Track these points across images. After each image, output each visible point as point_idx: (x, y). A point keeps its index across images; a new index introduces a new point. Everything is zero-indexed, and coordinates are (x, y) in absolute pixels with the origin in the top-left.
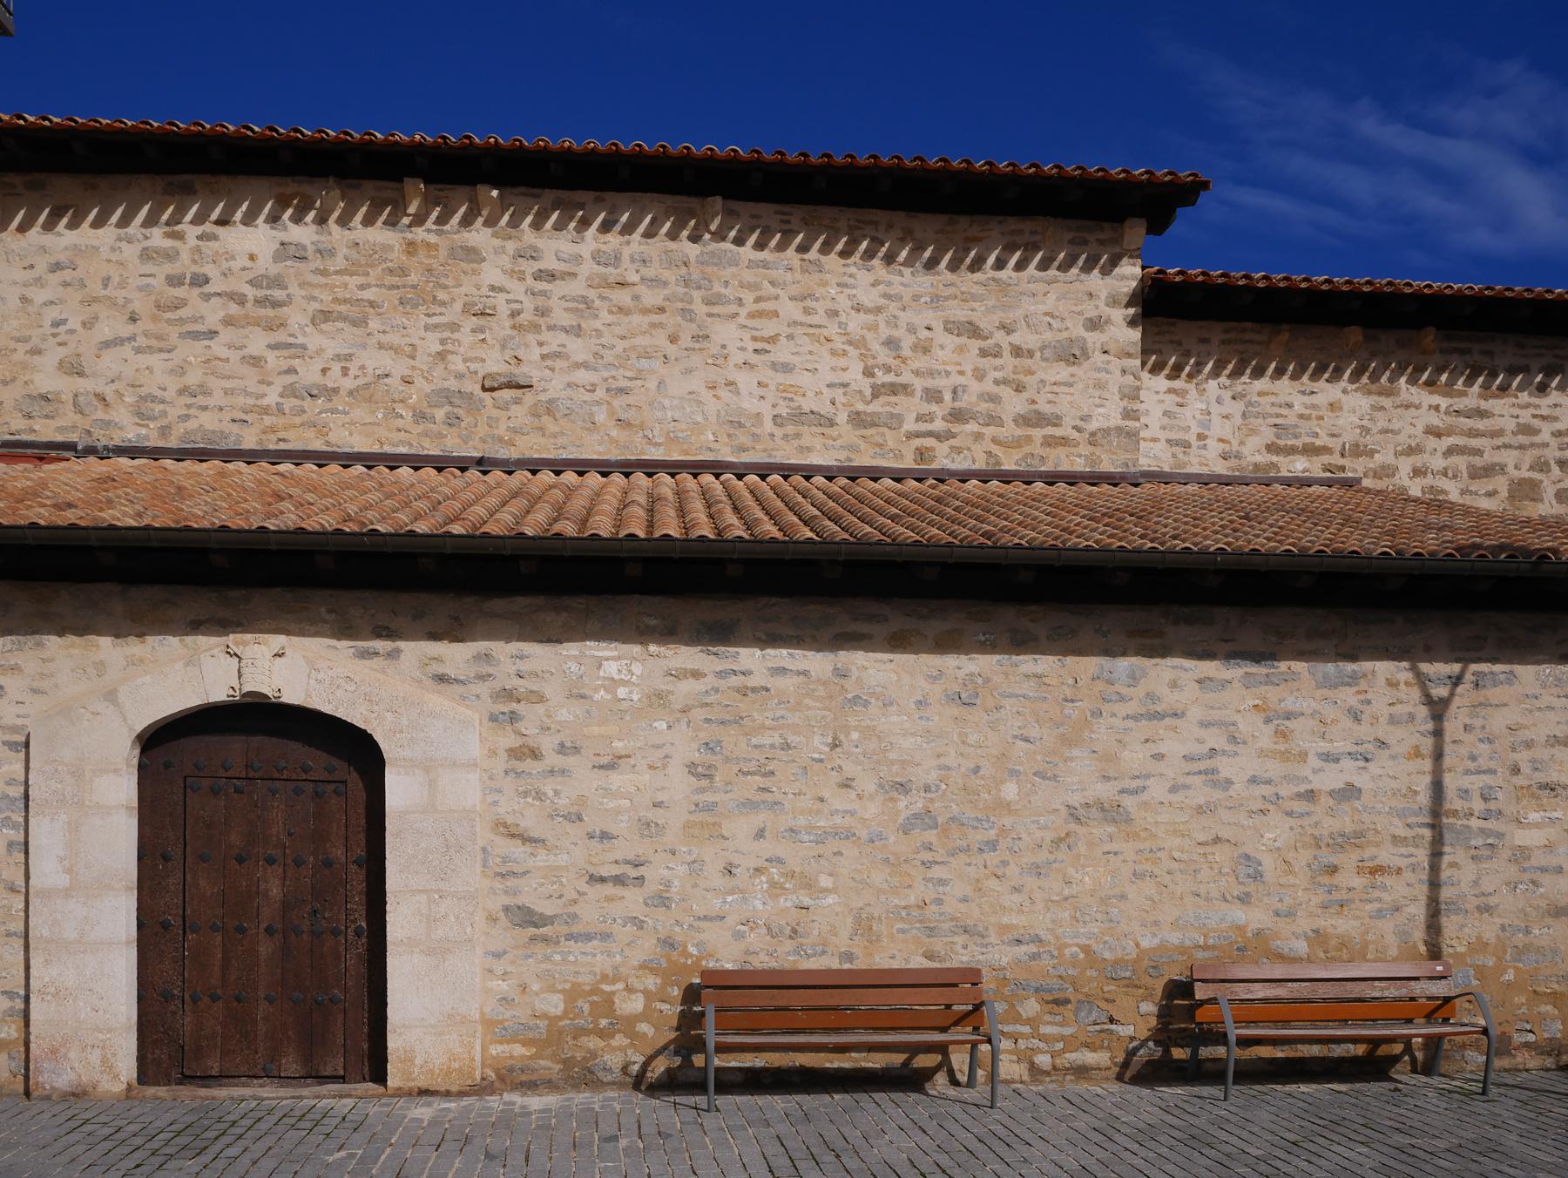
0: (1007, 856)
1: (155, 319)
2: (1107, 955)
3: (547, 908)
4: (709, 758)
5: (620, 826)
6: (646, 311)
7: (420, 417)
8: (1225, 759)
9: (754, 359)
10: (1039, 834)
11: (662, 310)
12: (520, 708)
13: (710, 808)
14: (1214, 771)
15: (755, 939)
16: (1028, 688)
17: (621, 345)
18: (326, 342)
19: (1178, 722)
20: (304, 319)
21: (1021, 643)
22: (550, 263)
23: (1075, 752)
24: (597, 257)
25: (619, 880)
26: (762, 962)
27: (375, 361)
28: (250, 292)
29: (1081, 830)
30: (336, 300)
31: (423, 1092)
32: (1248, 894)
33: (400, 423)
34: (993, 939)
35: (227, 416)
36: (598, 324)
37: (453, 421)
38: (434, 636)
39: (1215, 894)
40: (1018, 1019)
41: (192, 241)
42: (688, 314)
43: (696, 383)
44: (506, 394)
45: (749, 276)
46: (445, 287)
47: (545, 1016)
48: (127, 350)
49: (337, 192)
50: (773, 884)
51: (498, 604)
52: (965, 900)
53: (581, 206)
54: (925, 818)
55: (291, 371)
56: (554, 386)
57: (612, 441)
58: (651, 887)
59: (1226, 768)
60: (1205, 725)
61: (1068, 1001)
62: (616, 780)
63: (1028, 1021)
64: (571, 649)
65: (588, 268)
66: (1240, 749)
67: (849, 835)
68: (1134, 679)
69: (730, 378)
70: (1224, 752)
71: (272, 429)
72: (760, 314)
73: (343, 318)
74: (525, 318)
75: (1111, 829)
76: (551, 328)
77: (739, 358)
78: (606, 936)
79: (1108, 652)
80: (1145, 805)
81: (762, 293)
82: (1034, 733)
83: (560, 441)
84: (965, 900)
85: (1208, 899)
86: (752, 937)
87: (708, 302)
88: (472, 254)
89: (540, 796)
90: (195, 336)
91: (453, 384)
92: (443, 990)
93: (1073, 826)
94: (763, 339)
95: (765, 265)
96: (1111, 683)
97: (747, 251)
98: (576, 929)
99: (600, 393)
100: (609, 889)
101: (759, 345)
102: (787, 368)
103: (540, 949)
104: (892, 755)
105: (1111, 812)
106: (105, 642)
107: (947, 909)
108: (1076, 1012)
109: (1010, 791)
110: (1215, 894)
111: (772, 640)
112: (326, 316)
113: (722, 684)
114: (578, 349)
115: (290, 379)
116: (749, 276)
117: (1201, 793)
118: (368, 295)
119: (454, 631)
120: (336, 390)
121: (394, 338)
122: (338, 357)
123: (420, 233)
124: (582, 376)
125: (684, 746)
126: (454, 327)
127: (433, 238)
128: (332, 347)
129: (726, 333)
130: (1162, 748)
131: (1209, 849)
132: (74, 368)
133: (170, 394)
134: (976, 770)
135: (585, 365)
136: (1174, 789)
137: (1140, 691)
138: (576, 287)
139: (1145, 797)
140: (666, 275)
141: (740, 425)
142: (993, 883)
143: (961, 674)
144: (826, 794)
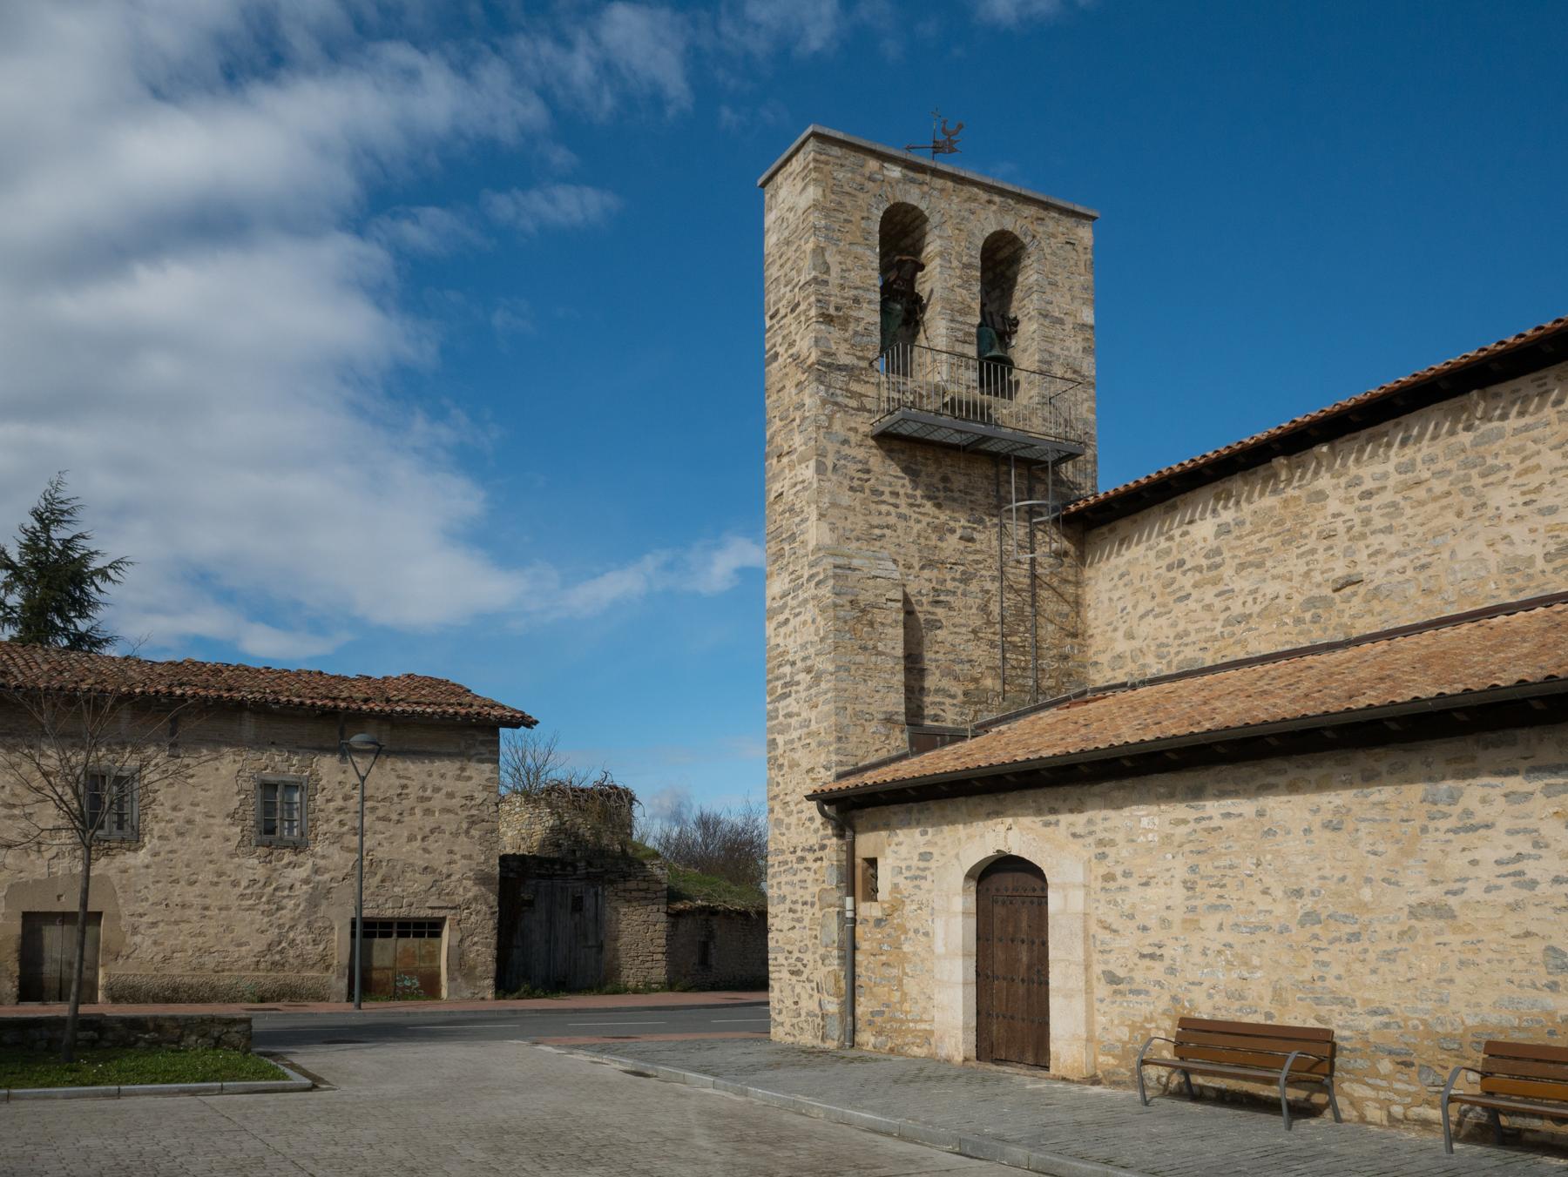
0: (1367, 945)
1: (1162, 594)
2: (1439, 1029)
3: (1121, 973)
4: (1192, 877)
5: (1152, 922)
6: (1435, 499)
7: (1298, 621)
8: (1531, 862)
9: (1523, 510)
10: (1389, 928)
11: (1449, 493)
12: (1106, 850)
13: (1193, 909)
14: (1521, 873)
15: (1219, 999)
16: (1375, 813)
17: (1420, 530)
18: (1242, 584)
19: (1490, 832)
20: (1231, 572)
21: (1370, 778)
22: (1369, 484)
23: (1411, 862)
24: (1401, 469)
25: (1152, 956)
26: (1222, 1016)
27: (1271, 588)
28: (1204, 562)
29: (1418, 925)
30: (1248, 554)
31: (1064, 1079)
32: (1555, 984)
33: (1286, 628)
34: (1358, 1010)
35: (1197, 647)
36: (1403, 520)
37: (1316, 619)
38: (1071, 811)
39: (1527, 981)
40: (1378, 1075)
41: (1177, 539)
42: (1468, 490)
43: (1479, 545)
44: (1348, 590)
45: (1514, 443)
46: (1307, 524)
47: (1119, 1040)
48: (1150, 618)
49: (1240, 483)
50: (1228, 962)
51: (1097, 789)
52: (1339, 978)
53: (1386, 434)
54: (1310, 918)
55: (1228, 608)
56: (1378, 575)
57: (1421, 607)
58: (1167, 962)
59: (1531, 869)
60: (1511, 832)
61: (1412, 1064)
62: (1150, 892)
63: (1384, 1078)
64: (1126, 812)
65: (1394, 479)
66: (1543, 852)
67: (1268, 929)
68: (1453, 799)
69: (1505, 533)
70: (1529, 856)
71: (1218, 651)
72: (1526, 471)
73: (1252, 564)
74: (1357, 529)
75: (1441, 923)
76: (1373, 533)
77: (1509, 513)
78: (1147, 993)
79: (1430, 779)
80: (1465, 903)
81: (1527, 453)
82: (1380, 848)
83: (1384, 617)
84: (1339, 978)
85: (1520, 986)
86: (1217, 997)
87: (1483, 475)
88: (1320, 496)
89: (1116, 904)
90: (1180, 599)
91: (1315, 592)
92: (1075, 1024)
93: (1413, 922)
94: (1530, 492)
95: (1527, 428)
96: (1435, 803)
97: (1513, 422)
98: (1134, 987)
99: (1410, 573)
100: (1147, 962)
101: (1527, 498)
102: (1552, 510)
103: (1119, 998)
104: (1290, 870)
105: (1442, 912)
106: (961, 827)
107: (1327, 984)
108: (1419, 1073)
109: (1366, 894)
110: (1527, 981)
111: (1222, 794)
112: (1242, 566)
113: (1198, 827)
114: (1392, 543)
115: (1227, 613)
116: (1514, 443)
117: (1510, 893)
118: (1264, 544)
119: (1078, 808)
120: (1250, 615)
121: (1280, 570)
122: (1251, 592)
123: (1290, 492)
124: (1397, 563)
125: (1181, 872)
126: (1313, 551)
127: (1297, 493)
128: (1247, 585)
129: (1500, 497)
130: (1477, 855)
131: (1520, 942)
132: (1130, 636)
133: (1170, 641)
134: (1343, 879)
135: (1398, 554)
136: (1488, 890)
137: (1457, 810)
138: (1387, 497)
139: (1464, 897)
140: (1451, 464)
141: (1517, 570)
142: (1357, 966)
143: (1331, 806)
144: (1254, 899)
